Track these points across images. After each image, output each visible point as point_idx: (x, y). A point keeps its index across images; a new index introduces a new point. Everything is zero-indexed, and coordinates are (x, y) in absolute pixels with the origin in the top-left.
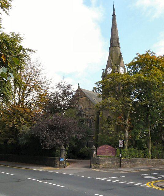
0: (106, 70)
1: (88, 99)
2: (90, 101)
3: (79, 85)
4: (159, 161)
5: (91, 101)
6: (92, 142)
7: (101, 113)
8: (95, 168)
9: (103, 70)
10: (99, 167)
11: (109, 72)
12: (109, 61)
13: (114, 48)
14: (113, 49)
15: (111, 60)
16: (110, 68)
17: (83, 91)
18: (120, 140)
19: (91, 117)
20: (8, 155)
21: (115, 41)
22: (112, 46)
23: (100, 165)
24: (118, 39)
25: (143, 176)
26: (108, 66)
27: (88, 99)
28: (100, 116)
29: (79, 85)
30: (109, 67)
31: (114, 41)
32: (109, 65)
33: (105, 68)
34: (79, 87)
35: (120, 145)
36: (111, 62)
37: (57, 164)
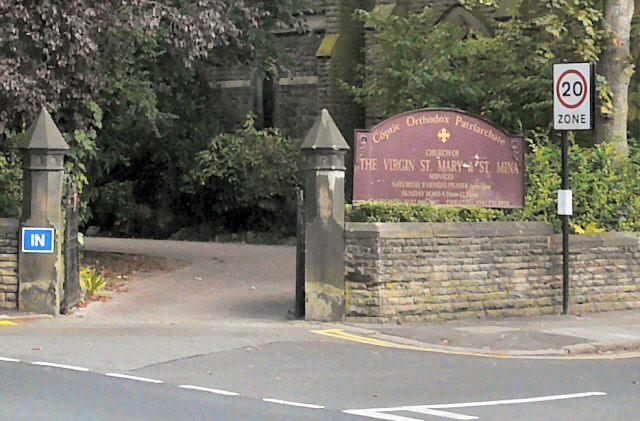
6: (312, 80)
10: (369, 312)
23: (381, 292)
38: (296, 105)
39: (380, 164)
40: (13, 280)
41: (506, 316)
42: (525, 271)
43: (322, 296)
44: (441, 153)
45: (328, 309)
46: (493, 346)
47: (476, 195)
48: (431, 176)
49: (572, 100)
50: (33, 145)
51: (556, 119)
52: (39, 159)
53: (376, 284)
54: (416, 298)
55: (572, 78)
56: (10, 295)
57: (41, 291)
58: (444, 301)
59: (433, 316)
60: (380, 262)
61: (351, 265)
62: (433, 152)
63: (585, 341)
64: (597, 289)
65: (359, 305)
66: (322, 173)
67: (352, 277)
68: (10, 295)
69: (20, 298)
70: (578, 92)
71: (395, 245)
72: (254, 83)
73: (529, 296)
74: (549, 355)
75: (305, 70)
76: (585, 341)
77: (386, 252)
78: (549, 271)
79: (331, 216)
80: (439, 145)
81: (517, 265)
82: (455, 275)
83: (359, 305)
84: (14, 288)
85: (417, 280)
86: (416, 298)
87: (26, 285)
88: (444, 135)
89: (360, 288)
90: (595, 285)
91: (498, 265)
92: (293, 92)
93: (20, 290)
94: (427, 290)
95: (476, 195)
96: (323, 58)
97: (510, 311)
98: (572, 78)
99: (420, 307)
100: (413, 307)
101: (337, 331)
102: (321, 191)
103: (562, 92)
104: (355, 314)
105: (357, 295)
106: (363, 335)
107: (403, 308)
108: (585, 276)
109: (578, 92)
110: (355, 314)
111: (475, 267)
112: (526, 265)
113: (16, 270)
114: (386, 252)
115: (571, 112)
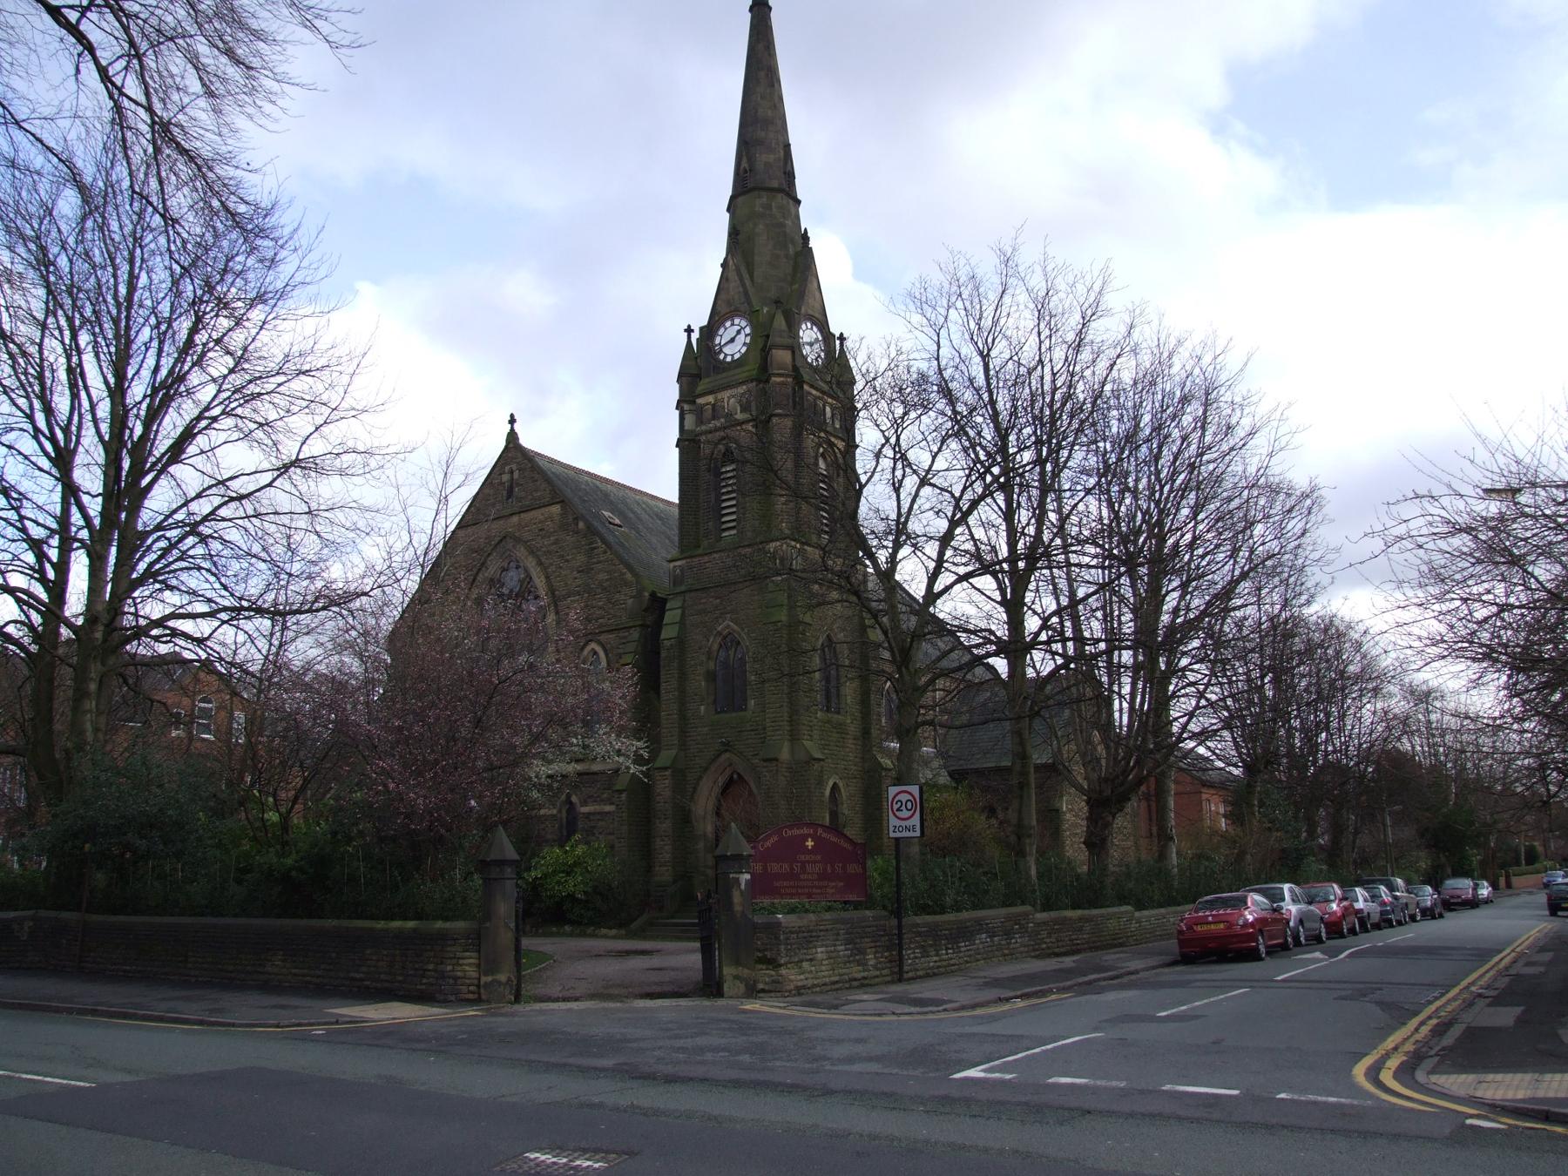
0: (709, 332)
1: (576, 519)
2: (592, 531)
3: (512, 421)
4: (1087, 927)
5: (595, 533)
6: (608, 808)
7: (672, 616)
8: (752, 992)
9: (689, 330)
10: (775, 989)
11: (735, 341)
12: (732, 275)
13: (760, 201)
14: (758, 209)
15: (746, 276)
16: (737, 321)
17: (542, 463)
18: (893, 790)
19: (603, 638)
20: (965, 915)
21: (771, 158)
22: (750, 185)
23: (783, 971)
24: (787, 146)
25: (447, 1014)
26: (723, 309)
27: (583, 518)
28: (668, 633)
29: (512, 421)
30: (731, 315)
31: (763, 158)
32: (729, 303)
33: (701, 319)
34: (512, 437)
35: (893, 821)
36: (743, 285)
37: (456, 978)
38: (594, 827)
39: (765, 868)
40: (475, 975)
41: (863, 986)
42: (873, 950)
43: (736, 977)
44: (808, 858)
45: (742, 987)
46: (96, 1010)
47: (833, 891)
48: (802, 877)
49: (905, 814)
50: (493, 856)
51: (891, 829)
52: (498, 870)
53: (781, 965)
54: (807, 975)
55: (904, 797)
56: (471, 988)
57: (500, 983)
58: (824, 977)
59: (818, 989)
60: (783, 947)
61: (760, 951)
62: (802, 857)
63: (950, 1001)
64: (917, 961)
65: (766, 983)
66: (734, 875)
67: (761, 960)
68: (471, 988)
69: (482, 991)
70: (909, 807)
71: (792, 932)
72: (560, 811)
73: (877, 969)
74: (927, 1013)
75: (602, 801)
76: (950, 1001)
77: (788, 939)
78: (888, 949)
79: (743, 912)
80: (806, 850)
81: (869, 945)
82: (834, 955)
83: (766, 983)
84: (476, 982)
85: (807, 960)
86: (807, 975)
87: (484, 979)
88: (810, 843)
89: (767, 969)
90: (916, 958)
91: (857, 946)
92: (592, 817)
93: (482, 983)
94: (813, 968)
95: (833, 891)
96: (621, 792)
97: (866, 982)
98: (904, 797)
99: (810, 983)
100: (805, 982)
101: (757, 1006)
102: (734, 890)
103: (895, 807)
104: (763, 991)
105: (764, 975)
106: (780, 1007)
107: (800, 984)
108: (911, 954)
109: (909, 807)
110: (763, 991)
111: (843, 947)
112: (873, 944)
113: (479, 966)
114: (788, 939)
115: (904, 823)
